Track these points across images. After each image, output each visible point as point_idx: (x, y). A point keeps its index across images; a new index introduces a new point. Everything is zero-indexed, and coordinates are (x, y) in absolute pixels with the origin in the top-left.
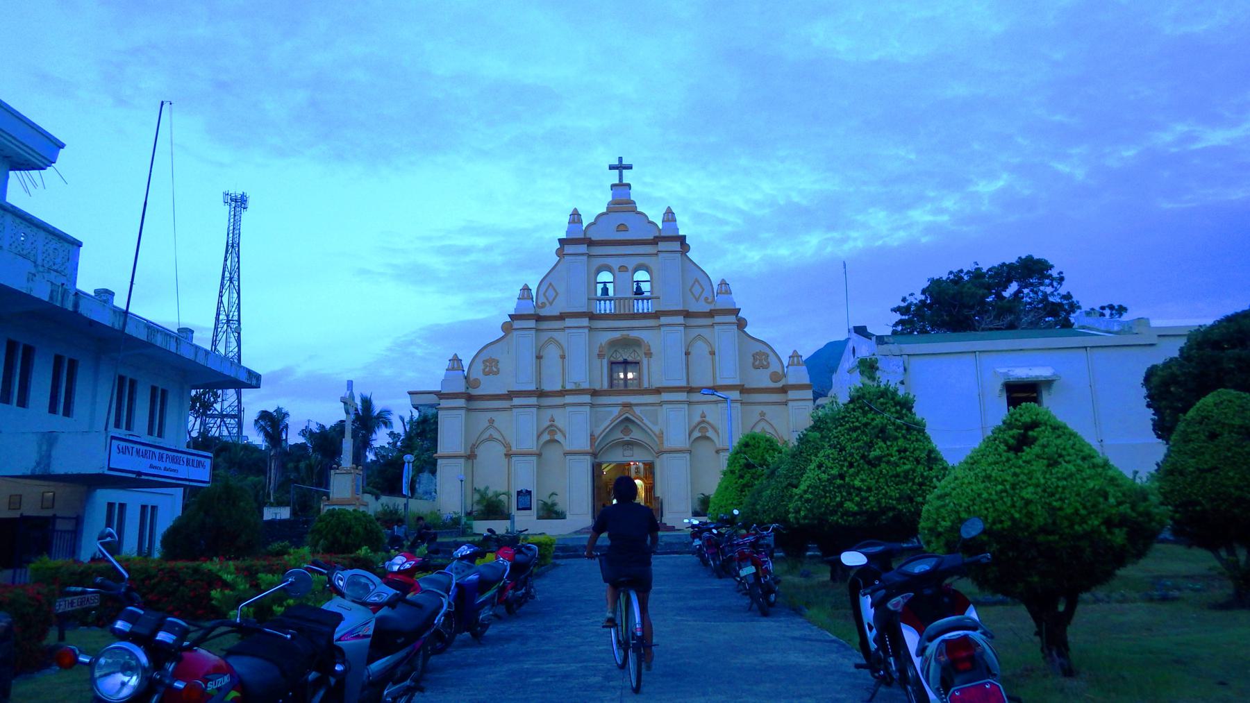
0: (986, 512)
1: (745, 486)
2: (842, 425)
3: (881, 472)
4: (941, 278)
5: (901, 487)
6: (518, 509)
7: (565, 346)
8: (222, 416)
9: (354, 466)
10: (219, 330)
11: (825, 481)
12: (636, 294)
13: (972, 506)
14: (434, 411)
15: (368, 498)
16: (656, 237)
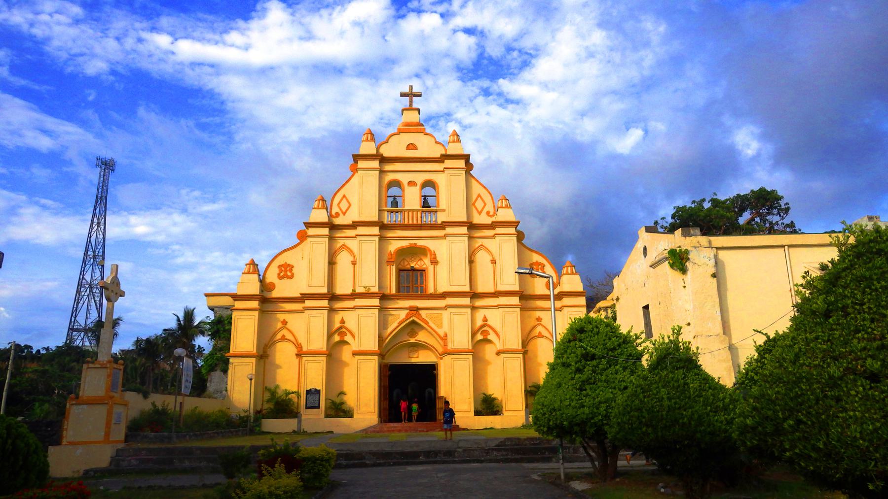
1: (587, 382)
4: (686, 206)
6: (307, 408)
7: (356, 251)
10: (87, 263)
14: (229, 312)
15: (132, 397)
16: (442, 155)
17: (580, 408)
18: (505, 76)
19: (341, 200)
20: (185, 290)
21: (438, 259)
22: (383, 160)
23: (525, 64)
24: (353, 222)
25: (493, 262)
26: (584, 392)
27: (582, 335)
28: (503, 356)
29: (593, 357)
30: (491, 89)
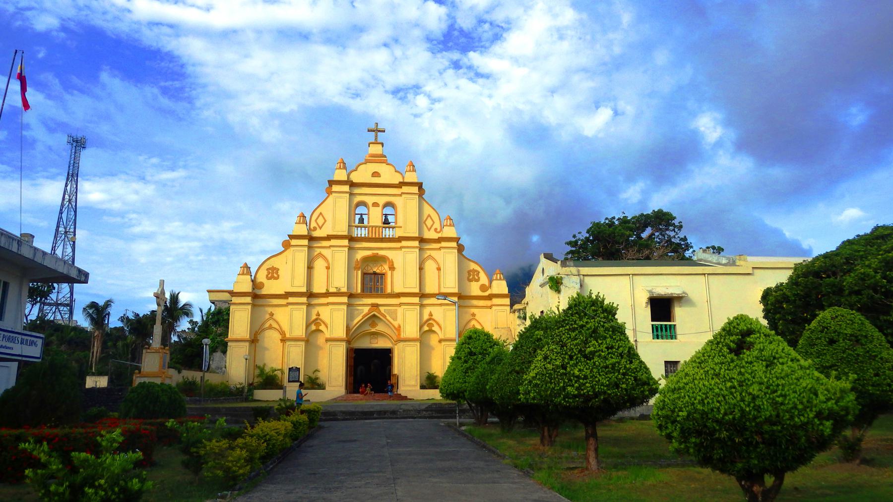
0: (718, 404)
2: (563, 326)
3: (594, 363)
5: (610, 376)
6: (289, 381)
8: (57, 305)
9: (163, 346)
10: (58, 239)
11: (550, 370)
12: (384, 223)
13: (706, 399)
14: (227, 305)
15: (172, 372)
16: (400, 183)
17: (464, 383)
18: (476, 49)
19: (319, 216)
20: (143, 260)
21: (395, 265)
22: (353, 185)
23: (497, 38)
24: (328, 235)
25: (439, 269)
26: (467, 374)
27: (470, 341)
28: (443, 343)
29: (475, 354)
30: (461, 62)
